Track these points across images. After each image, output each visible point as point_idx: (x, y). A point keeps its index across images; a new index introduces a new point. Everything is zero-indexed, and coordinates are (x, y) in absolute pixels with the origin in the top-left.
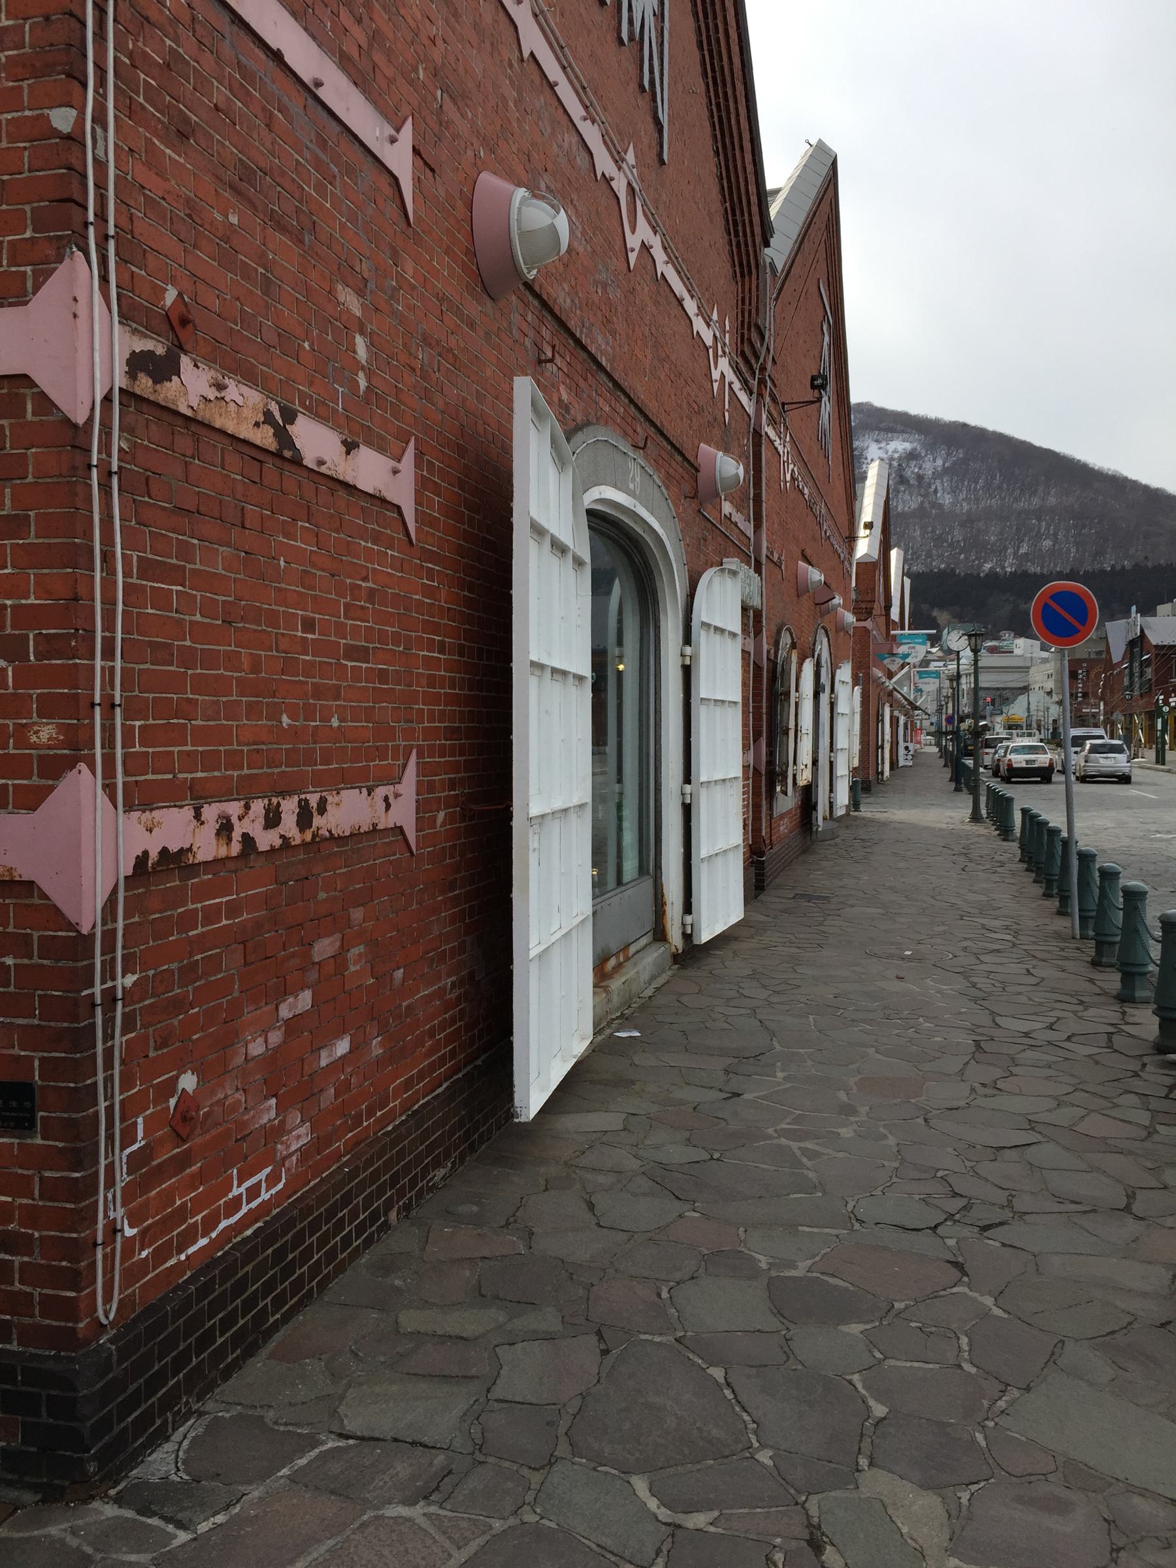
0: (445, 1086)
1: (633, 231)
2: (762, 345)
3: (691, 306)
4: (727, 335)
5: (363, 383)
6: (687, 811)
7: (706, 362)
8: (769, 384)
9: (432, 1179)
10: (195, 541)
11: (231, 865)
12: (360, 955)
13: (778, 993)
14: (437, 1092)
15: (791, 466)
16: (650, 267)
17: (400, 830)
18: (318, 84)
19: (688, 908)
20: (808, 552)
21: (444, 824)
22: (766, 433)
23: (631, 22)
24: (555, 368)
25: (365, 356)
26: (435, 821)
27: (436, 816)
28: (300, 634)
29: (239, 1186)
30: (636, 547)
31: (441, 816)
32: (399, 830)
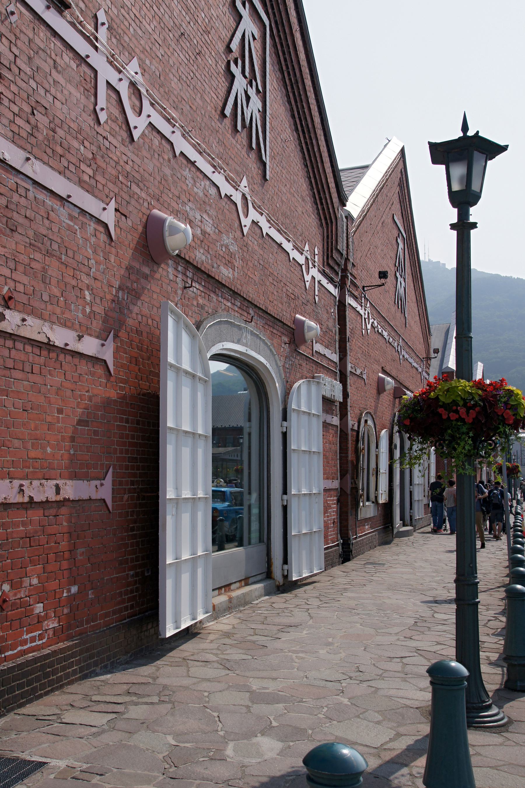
0: (127, 620)
1: (247, 216)
2: (342, 259)
3: (288, 246)
4: (316, 257)
5: (88, 310)
6: (285, 508)
7: (300, 273)
8: (350, 277)
9: (119, 659)
10: (13, 380)
11: (24, 506)
12: (83, 552)
13: (326, 603)
14: (123, 622)
15: (371, 321)
16: (258, 231)
17: (104, 500)
18: (69, 196)
19: (285, 561)
20: (387, 369)
21: (127, 501)
22: (349, 304)
23: (243, 119)
24: (195, 289)
25: (89, 299)
26: (123, 498)
27: (123, 497)
28: (56, 415)
29: (27, 635)
30: (253, 370)
31: (126, 497)
32: (102, 501)
